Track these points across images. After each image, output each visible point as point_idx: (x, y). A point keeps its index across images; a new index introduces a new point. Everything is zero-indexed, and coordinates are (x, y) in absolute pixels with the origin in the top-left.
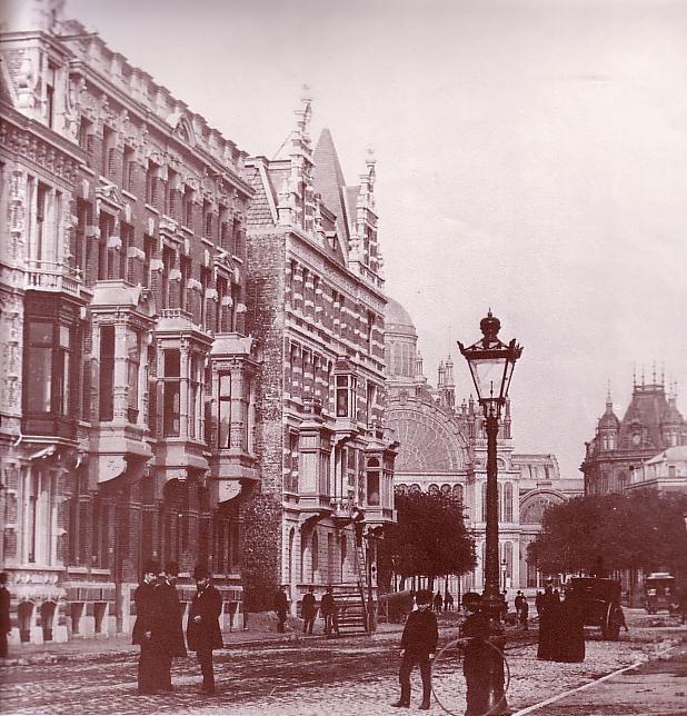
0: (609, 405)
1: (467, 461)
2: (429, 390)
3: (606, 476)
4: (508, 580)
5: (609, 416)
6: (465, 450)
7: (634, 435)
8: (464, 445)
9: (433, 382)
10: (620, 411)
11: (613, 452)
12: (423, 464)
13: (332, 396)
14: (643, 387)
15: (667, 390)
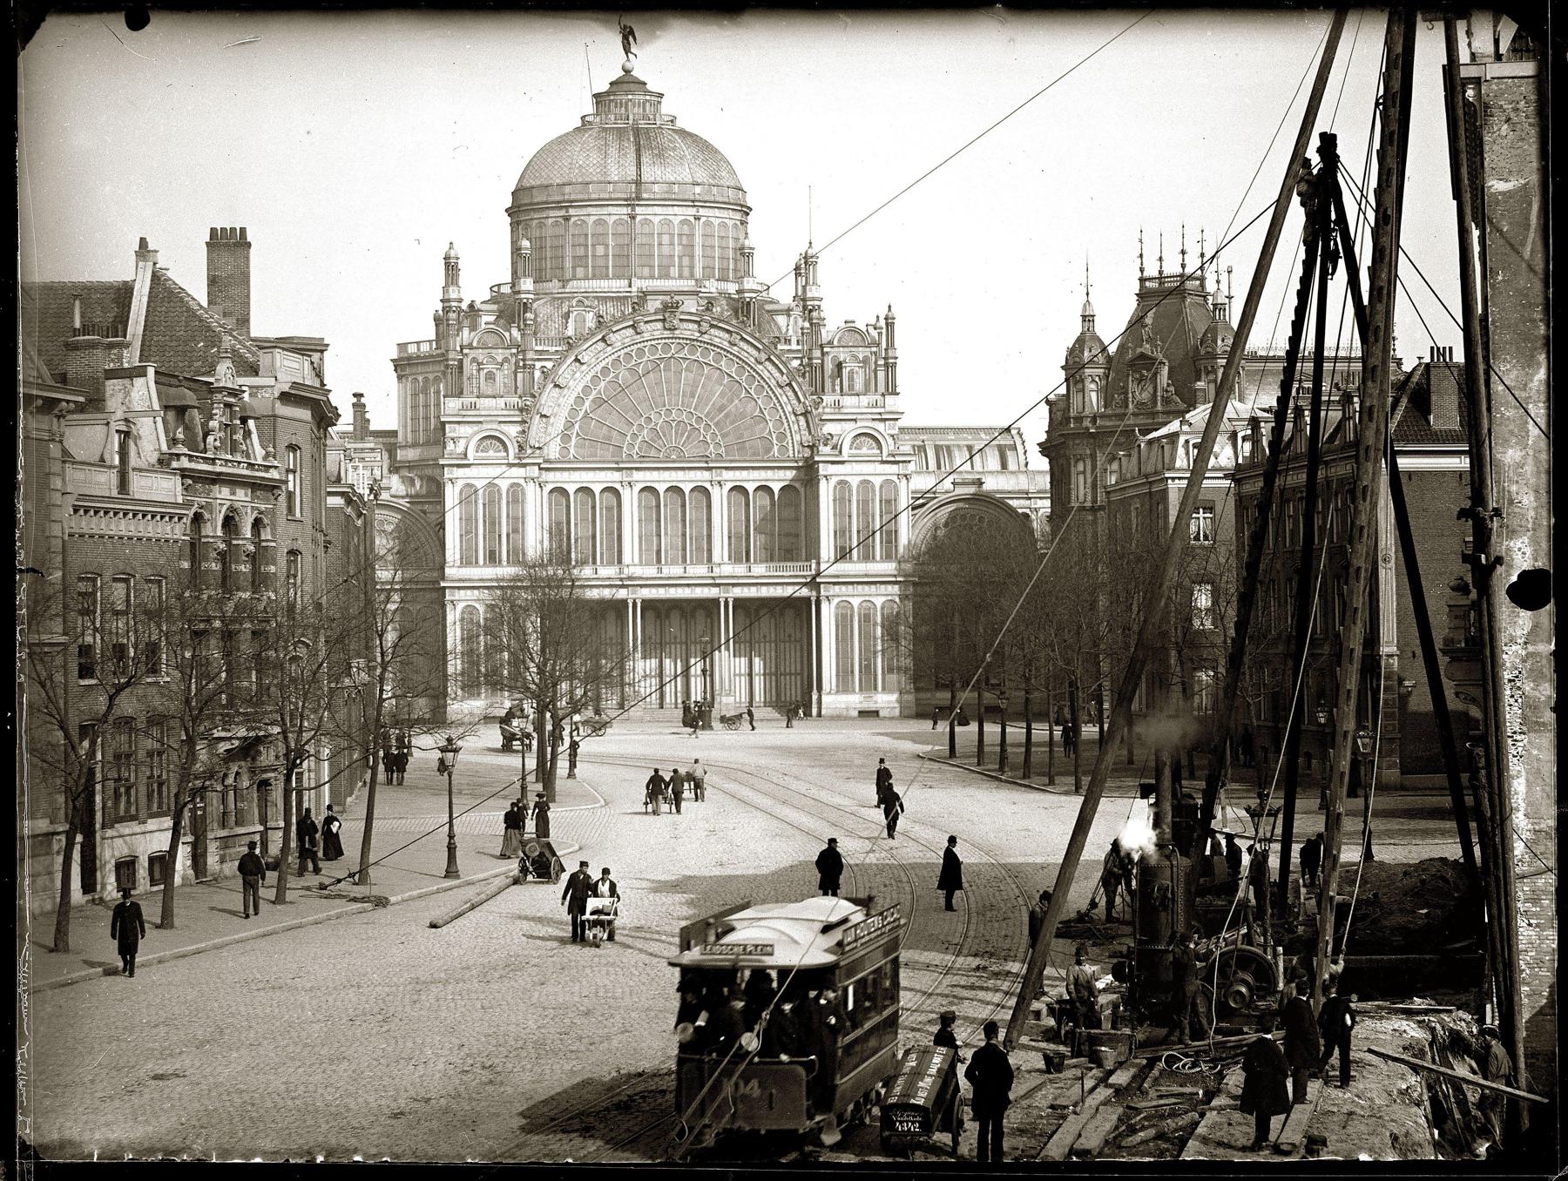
0: (1087, 319)
6: (802, 419)
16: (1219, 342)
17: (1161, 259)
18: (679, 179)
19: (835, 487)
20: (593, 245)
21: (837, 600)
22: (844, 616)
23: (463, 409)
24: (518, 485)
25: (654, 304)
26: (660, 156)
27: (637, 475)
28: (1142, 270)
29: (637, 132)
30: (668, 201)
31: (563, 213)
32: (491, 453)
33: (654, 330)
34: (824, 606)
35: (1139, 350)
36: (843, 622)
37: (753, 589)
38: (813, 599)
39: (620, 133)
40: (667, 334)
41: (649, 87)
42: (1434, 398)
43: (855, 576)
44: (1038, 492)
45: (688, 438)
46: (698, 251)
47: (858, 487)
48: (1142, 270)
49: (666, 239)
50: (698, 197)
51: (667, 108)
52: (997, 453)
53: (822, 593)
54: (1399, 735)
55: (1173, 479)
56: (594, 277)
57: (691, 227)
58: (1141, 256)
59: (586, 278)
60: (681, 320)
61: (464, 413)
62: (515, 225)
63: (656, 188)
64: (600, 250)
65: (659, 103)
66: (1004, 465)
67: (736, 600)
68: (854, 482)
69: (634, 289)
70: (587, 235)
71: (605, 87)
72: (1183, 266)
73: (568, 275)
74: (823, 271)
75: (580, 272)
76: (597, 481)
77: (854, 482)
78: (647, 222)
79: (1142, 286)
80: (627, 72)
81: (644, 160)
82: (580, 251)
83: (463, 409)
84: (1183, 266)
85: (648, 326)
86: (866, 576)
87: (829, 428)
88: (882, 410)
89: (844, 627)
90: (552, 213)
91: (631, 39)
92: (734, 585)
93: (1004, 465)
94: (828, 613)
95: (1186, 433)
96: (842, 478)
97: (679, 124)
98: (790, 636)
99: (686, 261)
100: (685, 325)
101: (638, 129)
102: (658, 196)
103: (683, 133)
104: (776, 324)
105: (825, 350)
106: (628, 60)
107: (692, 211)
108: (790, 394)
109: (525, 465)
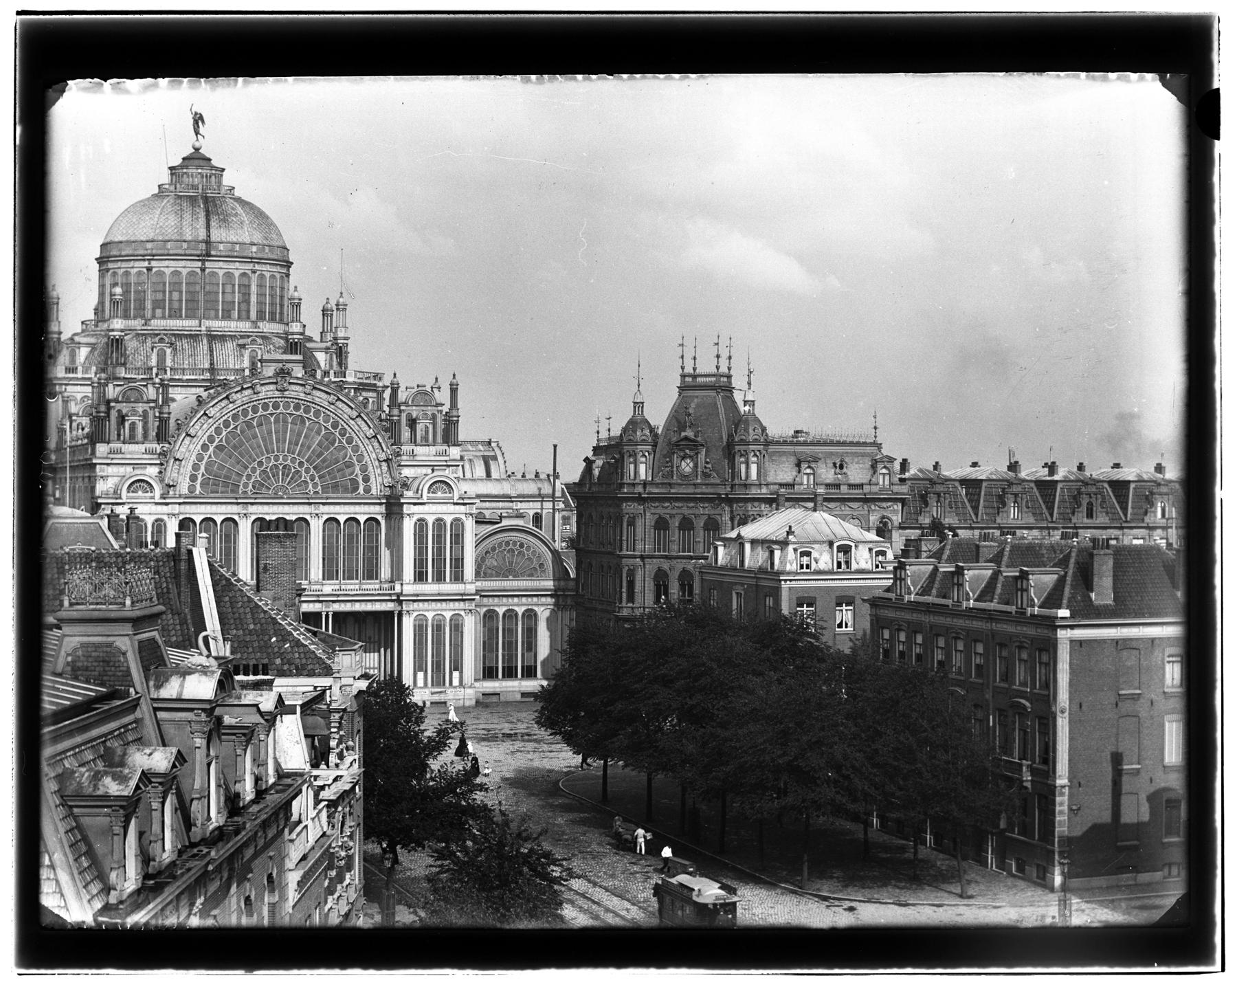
0: (638, 405)
1: (388, 481)
2: (309, 345)
3: (632, 523)
4: (456, 674)
5: (637, 422)
6: (384, 465)
7: (683, 458)
8: (383, 456)
9: (314, 331)
10: (658, 416)
11: (645, 484)
12: (315, 485)
13: (978, 666)
14: (695, 377)
15: (738, 382)
16: (751, 431)
17: (695, 358)
18: (240, 240)
19: (416, 523)
20: (170, 292)
21: (416, 614)
22: (420, 626)
23: (110, 453)
24: (162, 520)
25: (269, 371)
26: (225, 220)
27: (251, 509)
28: (683, 368)
29: (206, 200)
30: (229, 258)
31: (146, 264)
32: (140, 493)
33: (268, 391)
34: (405, 619)
35: (683, 434)
36: (420, 630)
37: (349, 605)
38: (396, 613)
39: (193, 200)
40: (277, 394)
41: (214, 163)
42: (1096, 579)
43: (432, 595)
44: (519, 496)
45: (292, 478)
46: (254, 299)
47: (434, 523)
48: (683, 368)
49: (229, 289)
50: (254, 255)
51: (227, 180)
52: (482, 462)
53: (404, 608)
54: (1067, 849)
55: (786, 580)
56: (170, 317)
57: (249, 278)
58: (682, 357)
59: (163, 317)
60: (290, 383)
61: (111, 456)
62: (103, 272)
63: (221, 247)
64: (176, 295)
65: (222, 175)
66: (488, 474)
67: (336, 614)
68: (430, 520)
69: (203, 328)
70: (164, 284)
71: (177, 161)
72: (718, 368)
73: (148, 314)
74: (352, 316)
75: (159, 312)
76: (219, 513)
77: (430, 520)
78: (214, 274)
79: (683, 381)
80: (197, 150)
81: (213, 224)
82: (159, 296)
83: (110, 453)
84: (718, 368)
85: (263, 388)
86: (439, 595)
87: (406, 472)
88: (447, 458)
89: (421, 636)
90: (137, 264)
91: (200, 124)
92: (334, 602)
93: (488, 474)
94: (408, 625)
95: (794, 543)
96: (422, 516)
97: (237, 193)
98: (370, 638)
99: (244, 306)
100: (293, 387)
101: (206, 197)
102: (223, 254)
103: (239, 200)
104: (316, 359)
105: (402, 408)
106: (197, 140)
107: (250, 266)
108: (376, 444)
109: (167, 504)
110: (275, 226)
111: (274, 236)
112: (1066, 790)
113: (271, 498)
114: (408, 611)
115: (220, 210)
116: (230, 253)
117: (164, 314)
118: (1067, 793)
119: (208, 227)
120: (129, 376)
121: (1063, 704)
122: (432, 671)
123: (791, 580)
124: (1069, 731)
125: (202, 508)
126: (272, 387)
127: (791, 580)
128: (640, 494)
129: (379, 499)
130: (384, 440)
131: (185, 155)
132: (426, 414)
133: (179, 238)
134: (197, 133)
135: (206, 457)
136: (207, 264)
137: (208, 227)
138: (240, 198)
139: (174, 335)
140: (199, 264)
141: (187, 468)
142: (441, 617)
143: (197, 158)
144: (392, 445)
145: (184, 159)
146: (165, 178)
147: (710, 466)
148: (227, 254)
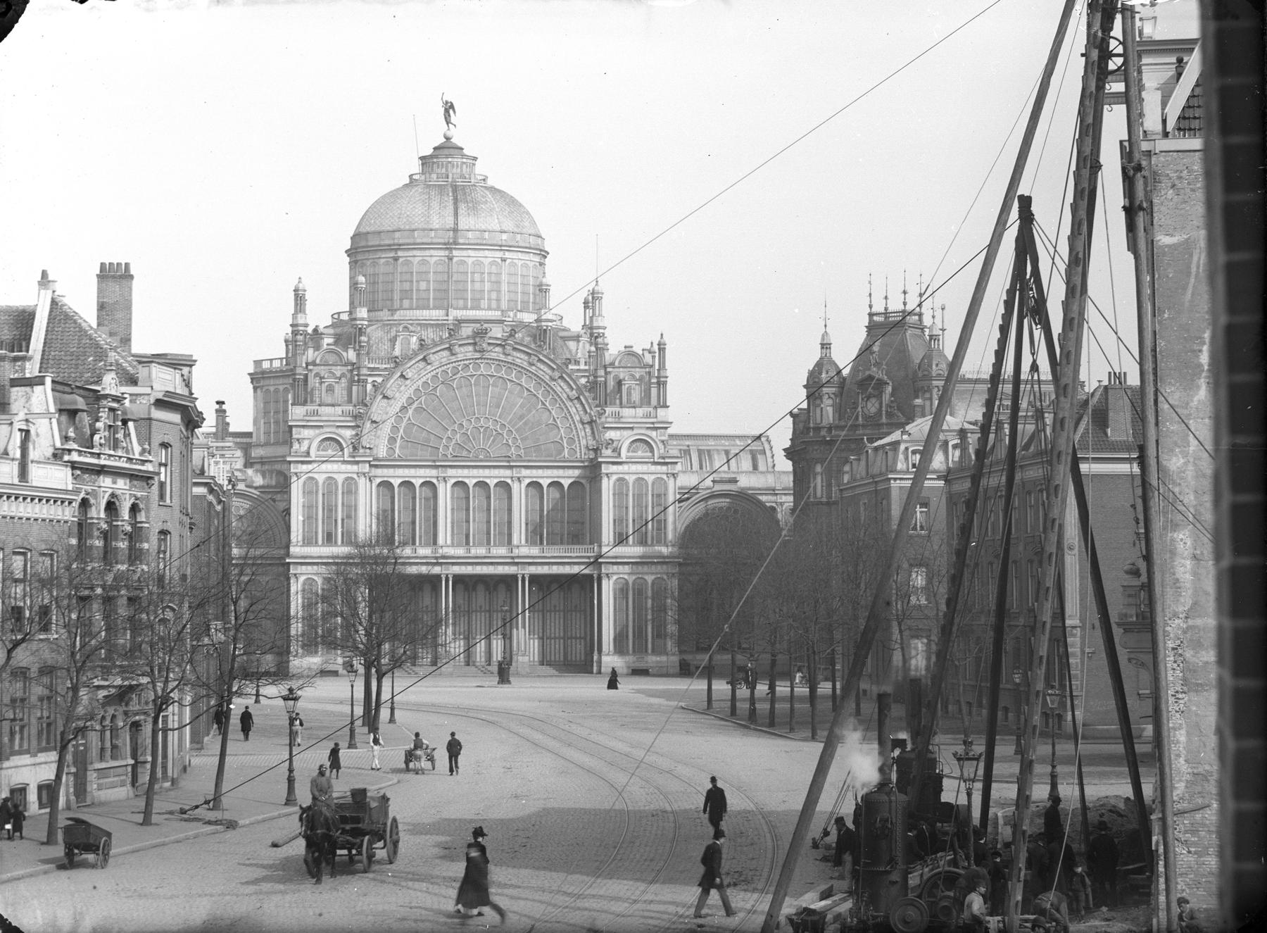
0: (825, 346)
20: (417, 281)
21: (615, 577)
26: (474, 208)
27: (451, 472)
28: (871, 307)
29: (455, 189)
31: (392, 254)
33: (466, 352)
34: (605, 582)
38: (595, 576)
41: (465, 152)
44: (783, 489)
48: (871, 307)
50: (504, 243)
51: (480, 169)
53: (603, 571)
55: (895, 479)
62: (354, 264)
63: (470, 235)
65: (474, 164)
66: (755, 467)
68: (631, 479)
69: (451, 318)
77: (631, 479)
80: (448, 139)
81: (460, 211)
85: (462, 349)
87: (611, 435)
88: (654, 420)
91: (451, 111)
92: (530, 564)
93: (755, 467)
95: (906, 441)
97: (490, 183)
102: (472, 242)
105: (608, 370)
107: (500, 254)
109: (357, 463)
110: (528, 213)
111: (527, 224)
112: (1078, 632)
113: (471, 461)
114: (607, 574)
115: (469, 198)
116: (479, 241)
117: (411, 303)
118: (1079, 634)
119: (456, 214)
120: (372, 366)
121: (1070, 541)
122: (634, 636)
123: (901, 479)
124: (1080, 569)
125: (400, 472)
126: (471, 348)
127: (901, 479)
128: (824, 437)
129: (582, 462)
130: (587, 400)
131: (436, 145)
132: (633, 375)
133: (426, 226)
134: (448, 122)
135: (405, 420)
136: (455, 253)
137: (456, 214)
138: (492, 187)
139: (420, 324)
140: (447, 253)
141: (386, 430)
142: (642, 581)
143: (447, 148)
144: (597, 406)
145: (435, 149)
146: (416, 167)
147: (895, 405)
148: (476, 242)
